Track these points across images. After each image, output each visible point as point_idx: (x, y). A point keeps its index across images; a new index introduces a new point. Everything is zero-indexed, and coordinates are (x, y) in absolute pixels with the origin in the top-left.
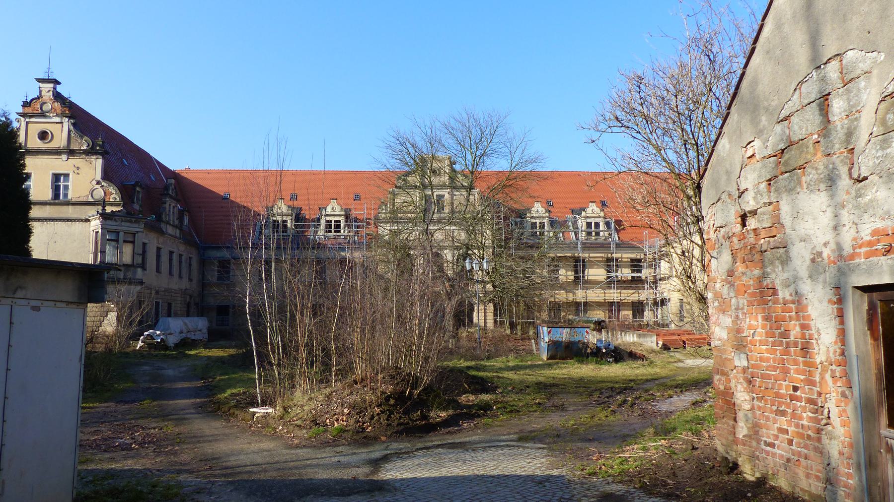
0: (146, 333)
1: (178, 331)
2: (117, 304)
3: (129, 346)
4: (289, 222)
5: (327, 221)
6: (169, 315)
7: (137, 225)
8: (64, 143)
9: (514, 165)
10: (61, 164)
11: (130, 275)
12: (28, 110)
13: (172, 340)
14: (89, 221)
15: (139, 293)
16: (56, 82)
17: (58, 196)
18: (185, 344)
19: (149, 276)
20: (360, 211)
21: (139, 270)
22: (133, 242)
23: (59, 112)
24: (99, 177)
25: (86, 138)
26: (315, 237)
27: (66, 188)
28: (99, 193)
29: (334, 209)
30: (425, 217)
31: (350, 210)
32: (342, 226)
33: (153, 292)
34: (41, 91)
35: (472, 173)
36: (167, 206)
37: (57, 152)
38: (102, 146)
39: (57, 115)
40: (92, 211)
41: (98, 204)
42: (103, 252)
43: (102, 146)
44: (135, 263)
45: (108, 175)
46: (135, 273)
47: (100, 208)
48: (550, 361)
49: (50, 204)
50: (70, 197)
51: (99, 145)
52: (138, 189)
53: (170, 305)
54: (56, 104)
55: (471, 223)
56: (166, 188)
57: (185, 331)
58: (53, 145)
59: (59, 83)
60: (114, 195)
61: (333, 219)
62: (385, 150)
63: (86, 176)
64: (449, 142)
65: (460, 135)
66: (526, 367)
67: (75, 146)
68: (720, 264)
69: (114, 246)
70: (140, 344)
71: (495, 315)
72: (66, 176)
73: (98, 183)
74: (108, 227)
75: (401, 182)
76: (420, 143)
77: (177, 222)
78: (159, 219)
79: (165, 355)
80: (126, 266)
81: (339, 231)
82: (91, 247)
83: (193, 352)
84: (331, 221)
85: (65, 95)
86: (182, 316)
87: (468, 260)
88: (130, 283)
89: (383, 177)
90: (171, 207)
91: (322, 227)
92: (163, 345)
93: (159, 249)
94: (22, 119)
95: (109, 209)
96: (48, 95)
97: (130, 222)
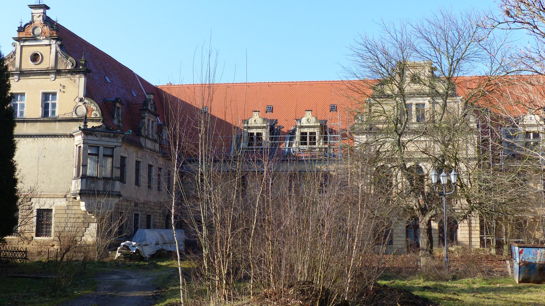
0: (122, 244)
1: (154, 242)
2: (97, 215)
3: (107, 256)
4: (264, 135)
5: (302, 134)
6: (148, 227)
7: (115, 140)
8: (52, 64)
9: (494, 69)
10: (49, 84)
11: (109, 188)
12: (23, 35)
13: (147, 252)
14: (73, 136)
15: (116, 204)
16: (46, 7)
17: (47, 115)
18: (163, 254)
19: (128, 189)
20: (337, 123)
21: (118, 183)
22: (112, 156)
23: (48, 35)
24: (81, 95)
25: (70, 58)
26: (289, 149)
27: (54, 105)
28: (82, 111)
29: (308, 121)
30: (399, 127)
31: (326, 121)
32: (317, 138)
33: (133, 204)
34: (33, 17)
35: (448, 79)
36: (146, 120)
37: (45, 73)
38: (84, 65)
39: (46, 38)
40: (75, 127)
41: (81, 121)
42: (85, 166)
43: (84, 65)
44: (114, 176)
45: (90, 93)
46: (113, 186)
47: (82, 124)
48: (523, 284)
49: (41, 121)
50: (57, 114)
51: (82, 64)
52: (118, 105)
53: (149, 217)
54: (45, 28)
55: (448, 132)
56: (145, 103)
57: (161, 242)
58: (44, 66)
59: (48, 8)
60: (96, 112)
61: (255, 131)
62: (353, 58)
63: (70, 95)
64: (424, 46)
65: (434, 39)
66: (495, 290)
67: (61, 67)
68: (414, 182)
69: (95, 161)
70: (118, 254)
71: (482, 233)
72: (54, 94)
73: (81, 100)
74: (90, 142)
75: (378, 90)
76: (392, 51)
77: (156, 137)
78: (137, 132)
79: (138, 265)
80: (106, 179)
81: (315, 144)
82: (74, 161)
83: (164, 264)
84: (306, 133)
85: (53, 18)
86: (161, 227)
87: (453, 173)
88: (109, 195)
89: (353, 87)
90: (149, 122)
91: (297, 139)
92: (138, 256)
93: (138, 163)
94: (18, 43)
95: (90, 125)
96: (39, 20)
97: (109, 136)
